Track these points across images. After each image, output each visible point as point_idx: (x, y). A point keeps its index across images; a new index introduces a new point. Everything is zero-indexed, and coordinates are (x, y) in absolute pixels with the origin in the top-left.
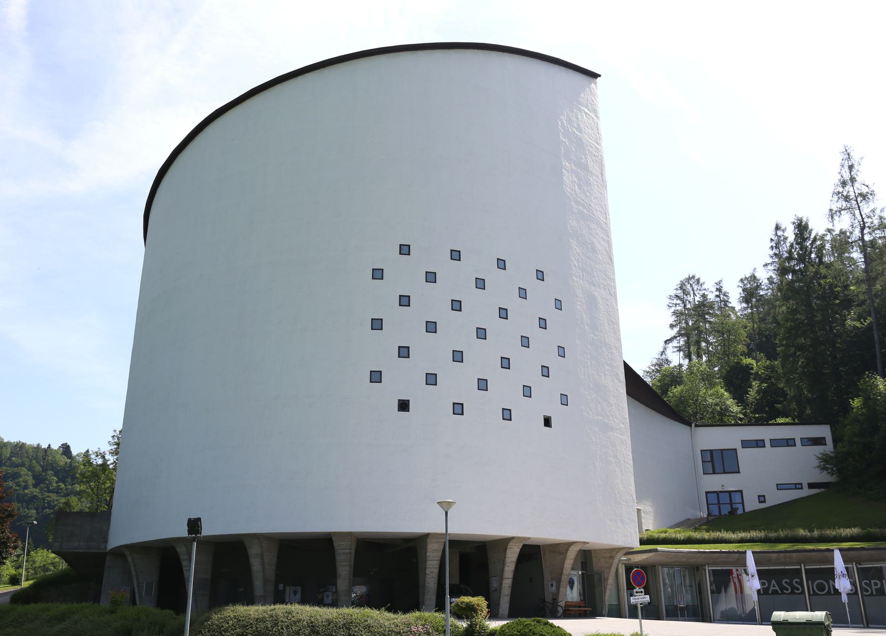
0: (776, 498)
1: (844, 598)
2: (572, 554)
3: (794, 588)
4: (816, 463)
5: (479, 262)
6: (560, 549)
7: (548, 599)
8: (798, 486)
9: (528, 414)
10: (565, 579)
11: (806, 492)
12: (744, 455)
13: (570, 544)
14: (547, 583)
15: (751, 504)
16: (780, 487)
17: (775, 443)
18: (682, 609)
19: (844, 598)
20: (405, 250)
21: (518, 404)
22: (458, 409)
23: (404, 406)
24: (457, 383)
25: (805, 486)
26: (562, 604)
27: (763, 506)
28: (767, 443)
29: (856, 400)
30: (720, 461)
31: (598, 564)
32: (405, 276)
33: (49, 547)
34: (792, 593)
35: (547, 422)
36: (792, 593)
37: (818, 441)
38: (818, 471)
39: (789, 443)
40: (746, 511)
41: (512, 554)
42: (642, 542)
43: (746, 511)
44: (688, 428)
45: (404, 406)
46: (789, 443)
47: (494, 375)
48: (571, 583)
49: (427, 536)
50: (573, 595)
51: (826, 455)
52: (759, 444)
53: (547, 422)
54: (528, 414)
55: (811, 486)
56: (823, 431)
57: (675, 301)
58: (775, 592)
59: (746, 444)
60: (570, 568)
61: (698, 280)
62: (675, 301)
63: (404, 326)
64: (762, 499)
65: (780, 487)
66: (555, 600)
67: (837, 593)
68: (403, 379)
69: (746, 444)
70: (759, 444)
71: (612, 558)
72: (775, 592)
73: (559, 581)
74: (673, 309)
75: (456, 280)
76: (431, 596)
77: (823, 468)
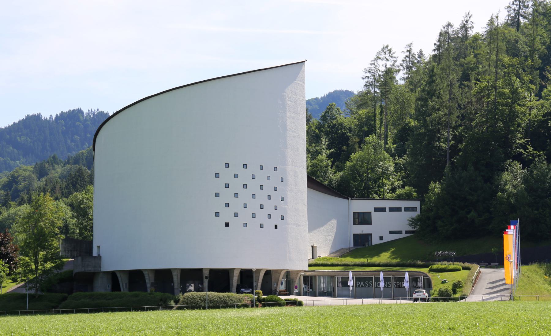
0: (389, 238)
1: (382, 289)
2: (283, 273)
3: (369, 285)
4: (408, 222)
5: (253, 169)
6: (278, 272)
7: (273, 289)
8: (400, 232)
9: (269, 224)
10: (280, 282)
11: (403, 235)
12: (375, 216)
13: (282, 270)
14: (273, 284)
15: (375, 241)
16: (391, 232)
17: (391, 209)
18: (325, 293)
19: (382, 289)
20: (227, 165)
21: (266, 221)
22: (245, 225)
23: (227, 225)
24: (245, 216)
25: (404, 232)
26: (278, 291)
27: (382, 242)
28: (387, 210)
29: (438, 185)
30: (362, 218)
31: (292, 276)
32: (227, 176)
33: (478, 304)
34: (369, 287)
35: (276, 227)
36: (369, 287)
37: (413, 209)
38: (408, 226)
39: (399, 209)
40: (373, 244)
41: (262, 274)
42: (310, 265)
43: (373, 244)
44: (347, 200)
45: (227, 225)
46: (399, 209)
47: (258, 211)
48: (282, 283)
49: (234, 269)
50: (282, 288)
51: (413, 219)
52: (383, 210)
53: (276, 227)
54: (269, 224)
55: (407, 232)
56: (416, 204)
57: (368, 75)
58: (362, 286)
59: (376, 210)
60: (282, 279)
61: (390, 50)
62: (368, 75)
63: (227, 196)
64: (381, 238)
65: (391, 232)
66: (276, 290)
67: (349, 286)
68: (227, 215)
69: (376, 210)
70: (383, 210)
71: (298, 274)
72: (362, 286)
73: (277, 283)
74: (366, 80)
75: (245, 176)
76: (234, 288)
77: (411, 225)
